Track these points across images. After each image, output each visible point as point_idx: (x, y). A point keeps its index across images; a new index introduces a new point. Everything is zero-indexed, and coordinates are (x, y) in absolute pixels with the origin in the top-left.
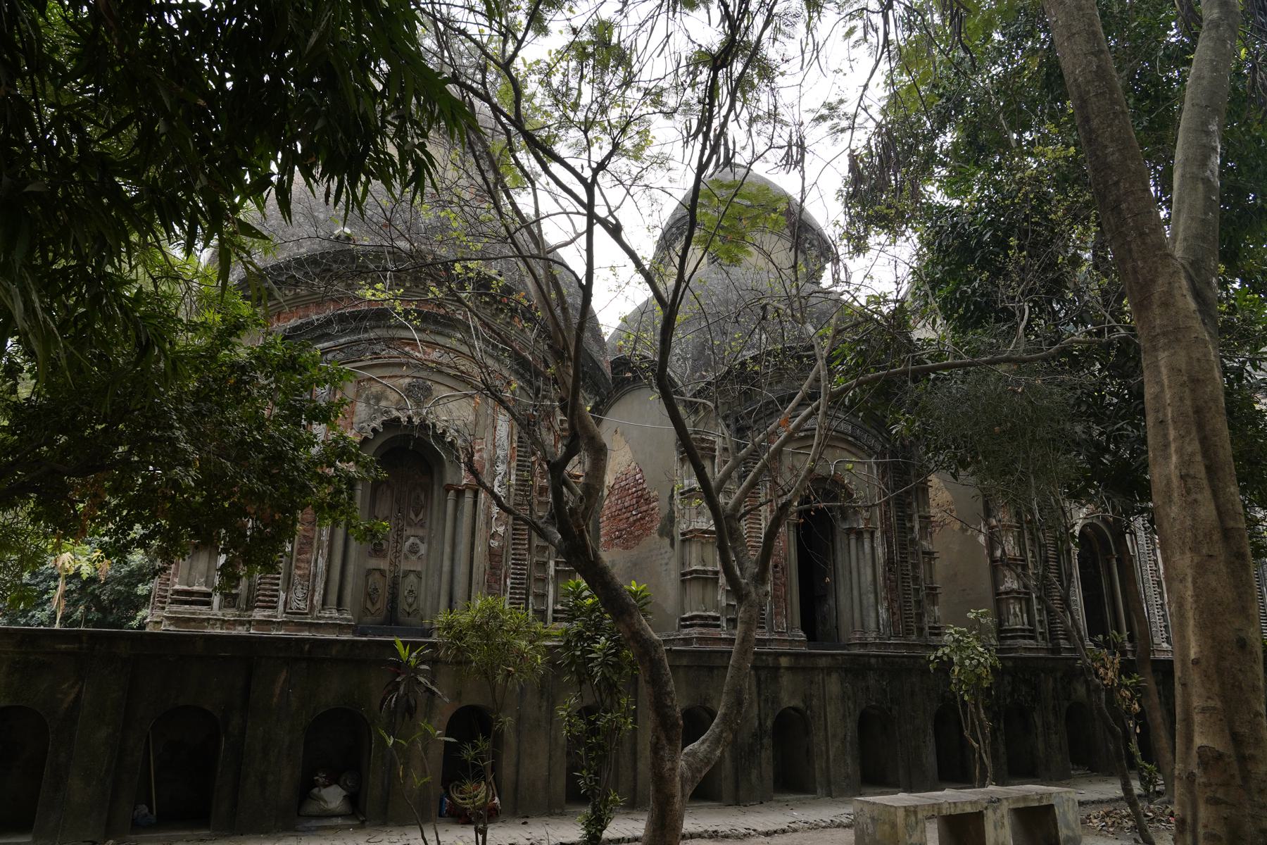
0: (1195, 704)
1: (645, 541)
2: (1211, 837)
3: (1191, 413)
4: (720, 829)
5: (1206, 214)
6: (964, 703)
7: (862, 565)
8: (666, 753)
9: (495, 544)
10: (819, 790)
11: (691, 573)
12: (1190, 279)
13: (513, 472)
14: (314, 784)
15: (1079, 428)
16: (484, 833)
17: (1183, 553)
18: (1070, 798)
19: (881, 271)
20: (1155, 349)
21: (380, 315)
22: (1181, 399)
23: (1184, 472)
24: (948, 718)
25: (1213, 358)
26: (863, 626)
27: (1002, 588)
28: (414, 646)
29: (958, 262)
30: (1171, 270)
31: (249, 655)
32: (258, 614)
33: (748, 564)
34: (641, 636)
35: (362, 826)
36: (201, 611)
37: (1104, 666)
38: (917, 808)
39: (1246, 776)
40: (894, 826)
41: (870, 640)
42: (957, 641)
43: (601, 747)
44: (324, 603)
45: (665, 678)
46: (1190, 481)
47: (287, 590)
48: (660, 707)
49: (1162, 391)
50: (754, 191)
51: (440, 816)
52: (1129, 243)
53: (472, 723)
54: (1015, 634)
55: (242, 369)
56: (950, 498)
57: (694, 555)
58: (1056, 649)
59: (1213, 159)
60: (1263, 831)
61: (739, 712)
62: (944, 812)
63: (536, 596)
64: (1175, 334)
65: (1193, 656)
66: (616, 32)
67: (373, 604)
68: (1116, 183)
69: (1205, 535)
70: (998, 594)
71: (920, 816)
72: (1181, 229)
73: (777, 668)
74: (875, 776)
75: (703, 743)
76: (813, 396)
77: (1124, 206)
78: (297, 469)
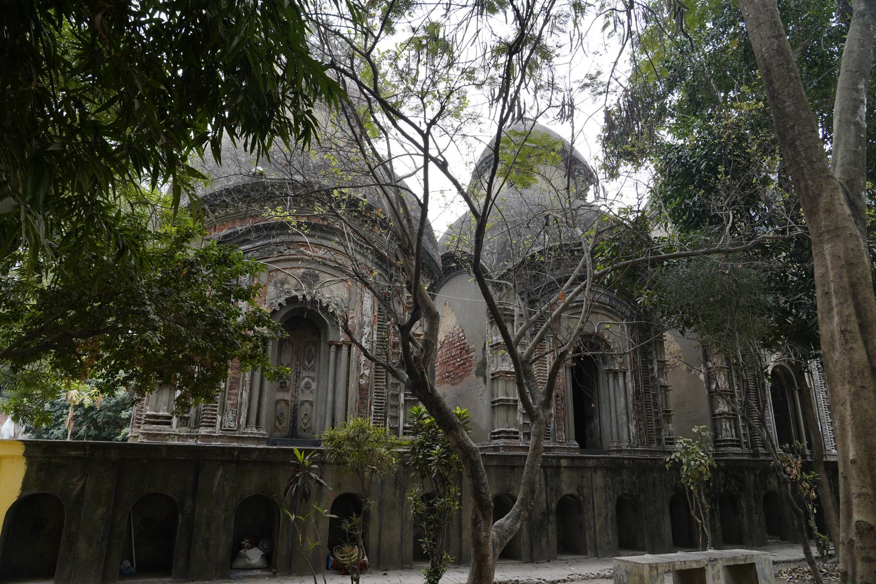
0: (854, 491)
1: (466, 380)
3: (847, 287)
5: (857, 147)
6: (691, 492)
7: (617, 395)
8: (482, 525)
9: (363, 382)
10: (589, 553)
11: (498, 401)
12: (846, 193)
14: (241, 547)
15: (770, 299)
17: (843, 385)
19: (628, 191)
20: (821, 242)
21: (283, 227)
22: (841, 277)
23: (843, 328)
24: (679, 502)
25: (863, 248)
27: (717, 411)
28: (307, 452)
29: (686, 185)
30: (832, 187)
31: (196, 459)
32: (203, 431)
33: (538, 395)
34: (464, 445)
35: (274, 575)
37: (790, 466)
40: (641, 577)
41: (624, 447)
42: (685, 448)
43: (437, 522)
44: (247, 423)
45: (481, 474)
47: (222, 414)
48: (478, 493)
49: (827, 271)
51: (327, 569)
53: (348, 505)
54: (726, 443)
55: (192, 264)
56: (679, 348)
57: (500, 389)
58: (756, 454)
59: (861, 108)
62: (677, 568)
63: (392, 417)
64: (836, 232)
65: (851, 458)
66: (442, 30)
67: (280, 424)
68: (792, 127)
69: (859, 373)
71: (660, 570)
73: (559, 467)
74: (628, 542)
75: (507, 519)
76: (582, 278)
77: (798, 143)
78: (229, 332)
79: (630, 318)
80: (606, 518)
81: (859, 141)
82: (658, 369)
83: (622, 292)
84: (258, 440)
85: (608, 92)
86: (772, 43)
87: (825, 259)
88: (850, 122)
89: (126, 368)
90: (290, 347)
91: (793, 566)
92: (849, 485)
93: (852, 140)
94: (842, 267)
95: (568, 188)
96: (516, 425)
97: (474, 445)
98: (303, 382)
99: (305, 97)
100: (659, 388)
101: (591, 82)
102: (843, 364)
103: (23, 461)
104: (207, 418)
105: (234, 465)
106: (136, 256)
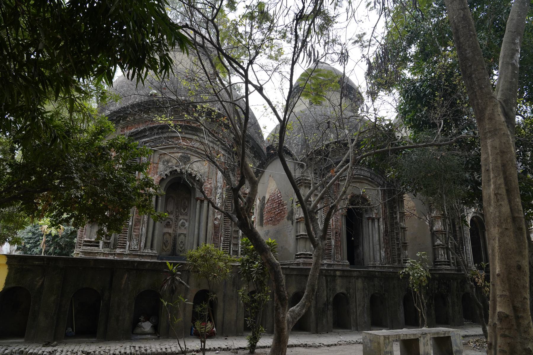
0: (498, 293)
1: (282, 222)
2: (502, 351)
3: (500, 166)
5: (512, 79)
6: (415, 292)
7: (374, 232)
8: (281, 310)
10: (352, 328)
11: (300, 235)
12: (502, 107)
13: (224, 193)
14: (139, 321)
15: (467, 175)
17: (495, 227)
18: (456, 334)
19: (385, 108)
20: (486, 138)
21: (164, 128)
22: (496, 160)
24: (408, 299)
25: (511, 142)
28: (175, 264)
29: (415, 101)
30: (494, 104)
31: (112, 268)
32: (118, 251)
33: (318, 232)
35: (158, 338)
36: (95, 249)
37: (478, 277)
39: (519, 325)
40: (379, 343)
41: (377, 265)
42: (412, 265)
43: (257, 308)
44: (145, 246)
45: (281, 279)
47: (130, 241)
49: (488, 157)
50: (326, 73)
52: (475, 92)
53: (202, 297)
54: (441, 263)
55: (103, 149)
56: (414, 205)
57: (301, 228)
58: (459, 270)
59: (516, 55)
61: (313, 294)
62: (401, 338)
63: (234, 244)
64: (495, 132)
65: (497, 272)
66: (266, 6)
67: (166, 247)
68: (470, 66)
69: (504, 220)
70: (434, 246)
71: (390, 340)
73: (335, 276)
74: (377, 324)
75: (297, 307)
76: (347, 161)
77: (473, 76)
78: (128, 190)
79: (383, 186)
81: (513, 75)
82: (400, 217)
85: (369, 45)
87: (487, 149)
88: (509, 63)
91: (477, 338)
92: (495, 289)
93: (509, 75)
97: (277, 262)
100: (400, 229)
101: (359, 40)
102: (495, 214)
106: (63, 143)
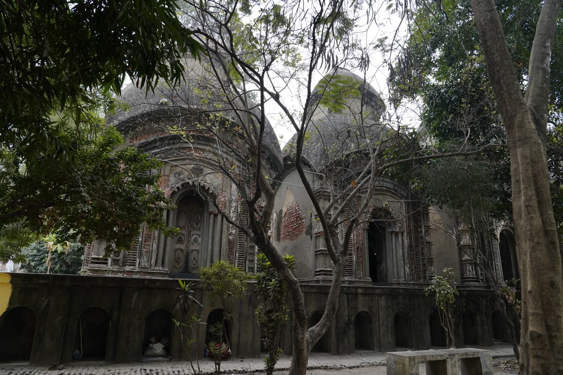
0: (530, 312)
4: (329, 365)
5: (543, 84)
6: (441, 311)
7: (398, 248)
8: (300, 331)
9: (231, 238)
10: (376, 349)
11: (320, 251)
12: (533, 114)
15: (496, 186)
16: (219, 365)
17: (526, 241)
18: (486, 355)
19: (409, 115)
21: (176, 138)
22: (527, 170)
23: (527, 204)
24: (435, 317)
25: (542, 151)
26: (398, 275)
27: (463, 259)
28: (187, 282)
29: (440, 110)
30: (523, 111)
31: (121, 286)
32: (128, 268)
33: (339, 247)
34: (289, 278)
35: (170, 361)
37: (508, 294)
38: (416, 359)
39: (552, 345)
40: (404, 365)
41: (402, 282)
42: (438, 282)
43: (274, 328)
44: (156, 263)
46: (530, 208)
47: (140, 258)
48: (297, 309)
49: (518, 167)
50: (346, 79)
51: (205, 357)
53: (216, 316)
54: (469, 279)
55: (112, 161)
56: (440, 218)
57: (321, 243)
58: (489, 287)
59: (547, 59)
60: (559, 371)
63: (250, 261)
64: (525, 140)
65: (529, 289)
66: (282, 9)
67: (178, 264)
68: (499, 71)
69: (536, 234)
70: (461, 261)
71: (416, 361)
72: (531, 91)
73: (357, 294)
74: (402, 343)
75: (317, 327)
76: (369, 172)
77: (502, 81)
78: (138, 204)
80: (387, 327)
81: (544, 80)
82: (425, 231)
83: (400, 180)
84: (163, 274)
85: (391, 50)
86: (487, 15)
87: (517, 158)
89: (74, 228)
90: (185, 215)
91: (508, 359)
92: (527, 307)
93: (540, 80)
94: (528, 164)
95: (361, 113)
96: (331, 267)
97: (296, 279)
98: (193, 238)
99: (176, 51)
100: (425, 244)
101: (381, 44)
102: (526, 227)
103: (10, 286)
104: (130, 260)
105: (145, 290)
106: (69, 155)
